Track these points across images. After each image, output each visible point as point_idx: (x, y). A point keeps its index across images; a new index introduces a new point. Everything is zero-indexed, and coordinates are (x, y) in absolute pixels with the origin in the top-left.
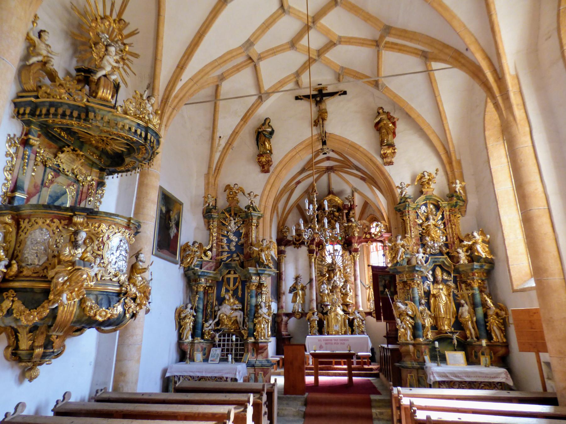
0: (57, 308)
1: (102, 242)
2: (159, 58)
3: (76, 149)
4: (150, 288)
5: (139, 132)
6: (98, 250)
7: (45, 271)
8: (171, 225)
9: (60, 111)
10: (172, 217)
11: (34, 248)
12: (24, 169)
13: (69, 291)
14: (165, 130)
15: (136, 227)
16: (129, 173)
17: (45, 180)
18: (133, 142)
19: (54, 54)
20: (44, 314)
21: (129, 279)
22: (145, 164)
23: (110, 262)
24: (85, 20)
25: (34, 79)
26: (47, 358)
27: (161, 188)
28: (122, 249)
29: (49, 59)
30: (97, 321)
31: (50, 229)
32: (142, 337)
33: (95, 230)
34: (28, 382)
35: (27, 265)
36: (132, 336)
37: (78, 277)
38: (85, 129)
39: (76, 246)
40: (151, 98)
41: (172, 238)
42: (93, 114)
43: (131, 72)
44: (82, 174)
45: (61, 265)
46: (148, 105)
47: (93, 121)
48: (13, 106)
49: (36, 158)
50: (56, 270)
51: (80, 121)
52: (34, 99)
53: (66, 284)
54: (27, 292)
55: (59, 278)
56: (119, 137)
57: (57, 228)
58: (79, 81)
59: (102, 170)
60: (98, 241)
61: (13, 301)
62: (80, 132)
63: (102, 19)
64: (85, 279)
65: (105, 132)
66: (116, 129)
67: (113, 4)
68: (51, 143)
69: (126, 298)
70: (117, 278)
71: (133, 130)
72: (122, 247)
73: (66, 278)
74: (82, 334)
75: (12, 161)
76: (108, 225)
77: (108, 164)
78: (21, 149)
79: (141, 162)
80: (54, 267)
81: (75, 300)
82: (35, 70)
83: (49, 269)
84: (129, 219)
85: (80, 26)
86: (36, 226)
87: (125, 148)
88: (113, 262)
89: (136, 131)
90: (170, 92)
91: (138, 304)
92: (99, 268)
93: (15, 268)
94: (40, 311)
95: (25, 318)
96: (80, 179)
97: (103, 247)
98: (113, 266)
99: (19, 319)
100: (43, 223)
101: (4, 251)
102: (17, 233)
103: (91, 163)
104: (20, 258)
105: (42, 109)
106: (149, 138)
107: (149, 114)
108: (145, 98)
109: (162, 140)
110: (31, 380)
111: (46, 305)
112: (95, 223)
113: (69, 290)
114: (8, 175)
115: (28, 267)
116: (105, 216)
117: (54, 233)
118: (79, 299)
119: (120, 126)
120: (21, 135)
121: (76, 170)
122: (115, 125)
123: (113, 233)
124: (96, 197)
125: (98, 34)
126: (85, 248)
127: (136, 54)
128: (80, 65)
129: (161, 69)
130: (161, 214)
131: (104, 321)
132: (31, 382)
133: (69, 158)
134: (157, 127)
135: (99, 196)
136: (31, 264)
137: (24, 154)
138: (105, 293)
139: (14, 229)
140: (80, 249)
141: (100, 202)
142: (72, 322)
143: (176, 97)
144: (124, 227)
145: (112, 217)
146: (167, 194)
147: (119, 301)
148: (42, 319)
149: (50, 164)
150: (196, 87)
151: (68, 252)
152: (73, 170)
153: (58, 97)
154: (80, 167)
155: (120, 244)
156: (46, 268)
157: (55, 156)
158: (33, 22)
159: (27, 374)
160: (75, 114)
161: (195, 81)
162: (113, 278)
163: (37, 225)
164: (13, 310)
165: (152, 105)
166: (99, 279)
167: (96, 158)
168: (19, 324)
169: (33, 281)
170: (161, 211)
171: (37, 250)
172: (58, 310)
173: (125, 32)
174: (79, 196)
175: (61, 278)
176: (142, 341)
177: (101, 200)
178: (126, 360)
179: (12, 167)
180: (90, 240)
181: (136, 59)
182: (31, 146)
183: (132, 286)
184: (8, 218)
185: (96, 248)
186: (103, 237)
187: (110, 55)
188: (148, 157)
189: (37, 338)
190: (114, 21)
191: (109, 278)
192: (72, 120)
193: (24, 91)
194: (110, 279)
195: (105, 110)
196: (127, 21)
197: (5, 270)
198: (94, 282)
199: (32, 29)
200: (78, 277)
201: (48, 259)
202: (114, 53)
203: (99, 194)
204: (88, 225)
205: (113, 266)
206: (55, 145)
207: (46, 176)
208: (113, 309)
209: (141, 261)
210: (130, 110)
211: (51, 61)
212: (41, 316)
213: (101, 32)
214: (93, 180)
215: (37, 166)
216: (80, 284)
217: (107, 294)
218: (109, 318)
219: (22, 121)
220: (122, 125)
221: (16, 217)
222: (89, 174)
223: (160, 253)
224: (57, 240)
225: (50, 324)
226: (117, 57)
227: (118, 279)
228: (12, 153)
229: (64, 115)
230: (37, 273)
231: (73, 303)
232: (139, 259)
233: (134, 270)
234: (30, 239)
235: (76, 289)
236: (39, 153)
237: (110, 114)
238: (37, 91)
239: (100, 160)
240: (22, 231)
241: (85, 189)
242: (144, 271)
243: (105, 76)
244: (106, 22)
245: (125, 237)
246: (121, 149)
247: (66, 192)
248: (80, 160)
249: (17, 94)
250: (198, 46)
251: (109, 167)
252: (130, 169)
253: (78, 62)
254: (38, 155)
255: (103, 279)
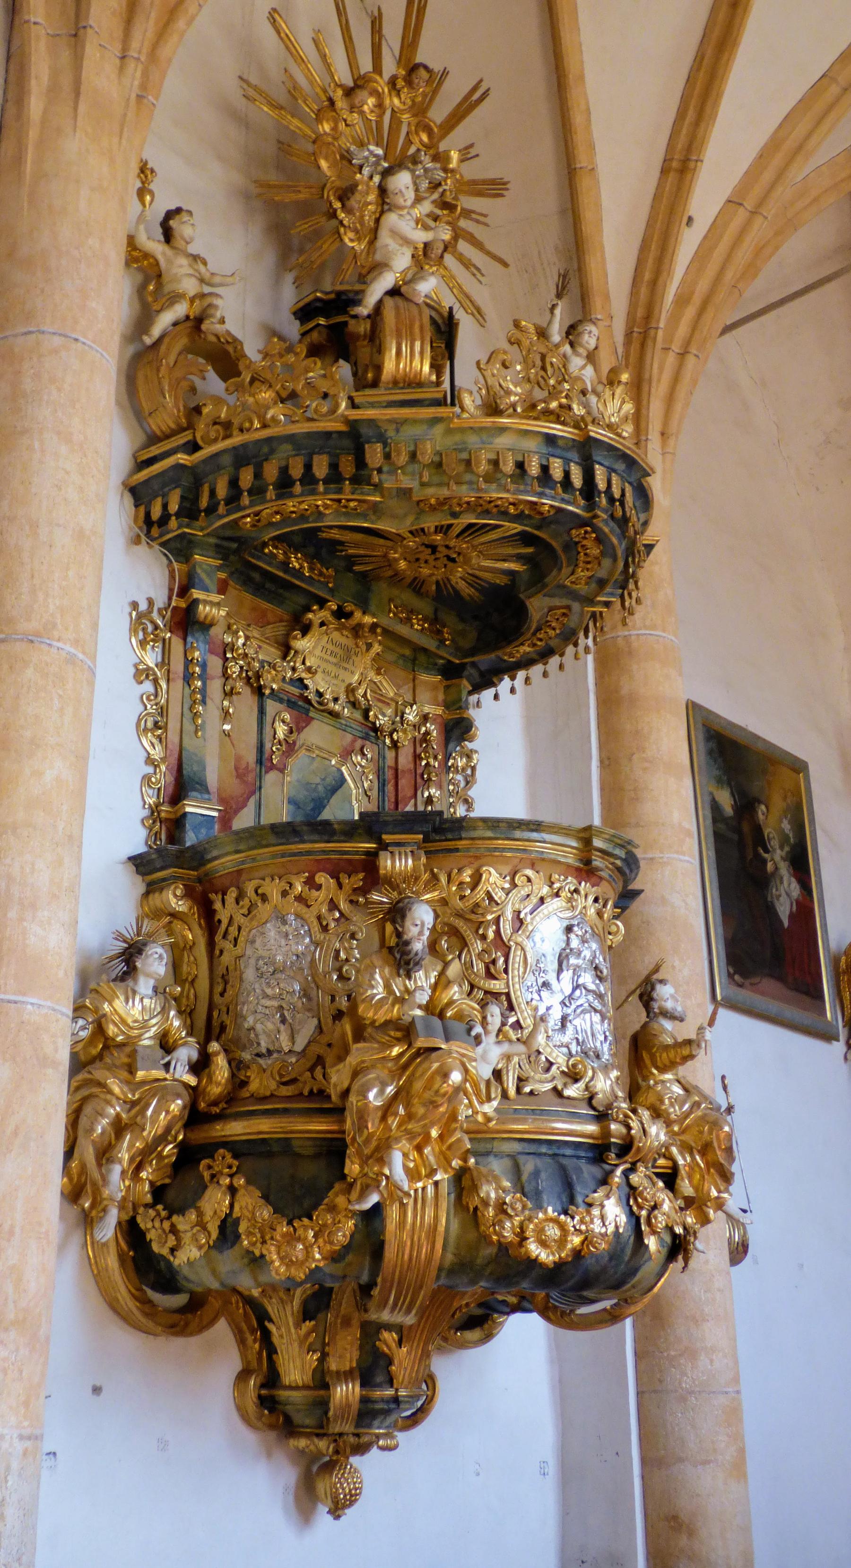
0: (377, 1208)
1: (500, 943)
2: (582, 161)
3: (349, 607)
4: (727, 1129)
5: (557, 473)
6: (490, 975)
7: (319, 1071)
8: (770, 866)
9: (271, 472)
10: (768, 831)
11: (269, 991)
12: (196, 715)
13: (410, 1140)
14: (663, 454)
15: (619, 869)
16: (554, 661)
17: (268, 745)
18: (544, 522)
19: (217, 280)
20: (342, 1237)
21: (633, 1093)
22: (607, 604)
23: (543, 1019)
24: (295, 123)
25: (175, 386)
26: (376, 1423)
27: (693, 709)
28: (580, 962)
29: (208, 300)
30: (533, 1263)
31: (310, 915)
32: (736, 1362)
33: (462, 898)
34: (329, 1518)
35: (258, 1055)
36: (692, 1354)
37: (431, 1079)
38: (364, 516)
39: (407, 963)
40: (580, 328)
41: (786, 923)
42: (379, 447)
43: (487, 259)
44: (382, 700)
45: (365, 1040)
46: (576, 363)
47: (384, 477)
48: (129, 500)
49: (225, 668)
50: (352, 1060)
51: (340, 491)
52: (186, 457)
53: (396, 1114)
54: (270, 1155)
55: (369, 1090)
56: (487, 513)
57: (333, 905)
58: (314, 351)
59: (450, 672)
60: (484, 937)
61: (232, 1190)
62: (348, 537)
63: (349, 92)
64: (459, 1089)
65: (433, 509)
66: (470, 483)
67: (376, 24)
68: (265, 605)
69: (633, 1169)
70: (581, 1085)
71: (534, 470)
72: (579, 954)
73: (390, 1090)
74: (488, 1337)
75: (156, 696)
76: (506, 869)
77: (466, 643)
78: (177, 645)
79: (591, 601)
80: (345, 1051)
81: (438, 1177)
82: (172, 359)
83: (329, 1061)
84: (586, 836)
85: (284, 147)
86: (264, 910)
87: (519, 558)
88: (556, 1014)
89: (545, 469)
90: (654, 284)
91: (689, 1202)
92: (505, 1048)
93: (221, 1068)
94: (325, 1225)
95: (278, 1253)
96: (382, 721)
97: (506, 961)
98: (559, 1038)
99: (262, 1256)
100: (285, 894)
101: (180, 1012)
102: (211, 944)
103: (407, 652)
104: (230, 1032)
105: (215, 484)
106: (602, 485)
107: (584, 393)
108: (556, 338)
109: (656, 484)
110: (337, 1510)
111: (341, 1201)
112: (460, 870)
113: (411, 1135)
114: (153, 745)
115: (261, 1061)
116: (489, 834)
117: (325, 929)
118: (452, 1173)
119: (483, 467)
120: (170, 599)
121: (361, 691)
122: (462, 468)
123: (534, 900)
124: (450, 782)
125: (346, 158)
126: (439, 968)
127: (493, 182)
128: (309, 294)
129: (598, 206)
130: (715, 821)
131: (559, 1265)
132: (337, 1517)
133: (330, 647)
134: (627, 430)
135: (459, 777)
136: (270, 1052)
137: (188, 662)
138: (544, 1149)
139: (198, 931)
140: (421, 974)
141: (466, 801)
142: (440, 1269)
143: (682, 301)
144: (569, 869)
145: (518, 834)
146: (728, 733)
147: (604, 1181)
148: (335, 1258)
149: (273, 681)
150: (760, 229)
151: (381, 989)
152: (350, 690)
153: (257, 424)
154: (372, 675)
155: (568, 943)
156: (320, 1061)
157: (286, 649)
158: (141, 193)
159: (322, 1486)
160: (321, 468)
161: (749, 204)
162: (565, 1085)
163: (268, 907)
164: (237, 1222)
165: (591, 358)
166: (512, 1092)
167: (423, 629)
168: (263, 1278)
169: (286, 1111)
170: (715, 807)
171: (280, 997)
172: (383, 1221)
173: (438, 114)
174: (390, 788)
175: (375, 1091)
176: (736, 1379)
177: (470, 793)
178: (681, 1460)
179: (162, 715)
180: (454, 939)
181: (499, 200)
182: (205, 626)
183: (645, 1114)
184: (175, 896)
185: (479, 967)
186: (497, 921)
187: (401, 208)
188: (611, 573)
189: (333, 1338)
190: (392, 82)
191: (549, 1086)
192: (313, 492)
193: (153, 439)
194: (555, 1089)
195: (415, 421)
196: (436, 66)
197: (192, 1081)
198: (495, 1104)
199: (141, 218)
200: (431, 1079)
201: (320, 1029)
202: (410, 195)
203: (457, 771)
204: (435, 877)
205: (559, 1038)
206: (279, 611)
207: (268, 730)
208: (589, 1213)
209: (666, 1014)
210: (508, 393)
211: (216, 307)
212: (331, 1243)
213: (354, 143)
214: (425, 718)
215: (234, 697)
216: (442, 1109)
217: (554, 1150)
218: (577, 1254)
219: (163, 545)
220: (489, 461)
221: (199, 888)
222: (409, 697)
223: (744, 995)
224: (337, 952)
225: (365, 1278)
226: (426, 207)
227: (587, 1088)
228: (152, 665)
229: (284, 484)
230: (294, 1081)
231: (430, 1190)
232: (655, 1006)
233: (645, 1055)
234: (252, 961)
235: (434, 1133)
236: (232, 647)
237: (439, 429)
238: (191, 426)
239: (439, 632)
240: (225, 936)
241: (405, 760)
242: (686, 1052)
243: (394, 292)
244: (364, 103)
245: (583, 913)
246: (506, 565)
247: (343, 780)
248: (369, 646)
249: (135, 457)
250: (735, 44)
251: (473, 655)
252: (552, 643)
253: (298, 283)
254: (229, 655)
255: (527, 1090)
